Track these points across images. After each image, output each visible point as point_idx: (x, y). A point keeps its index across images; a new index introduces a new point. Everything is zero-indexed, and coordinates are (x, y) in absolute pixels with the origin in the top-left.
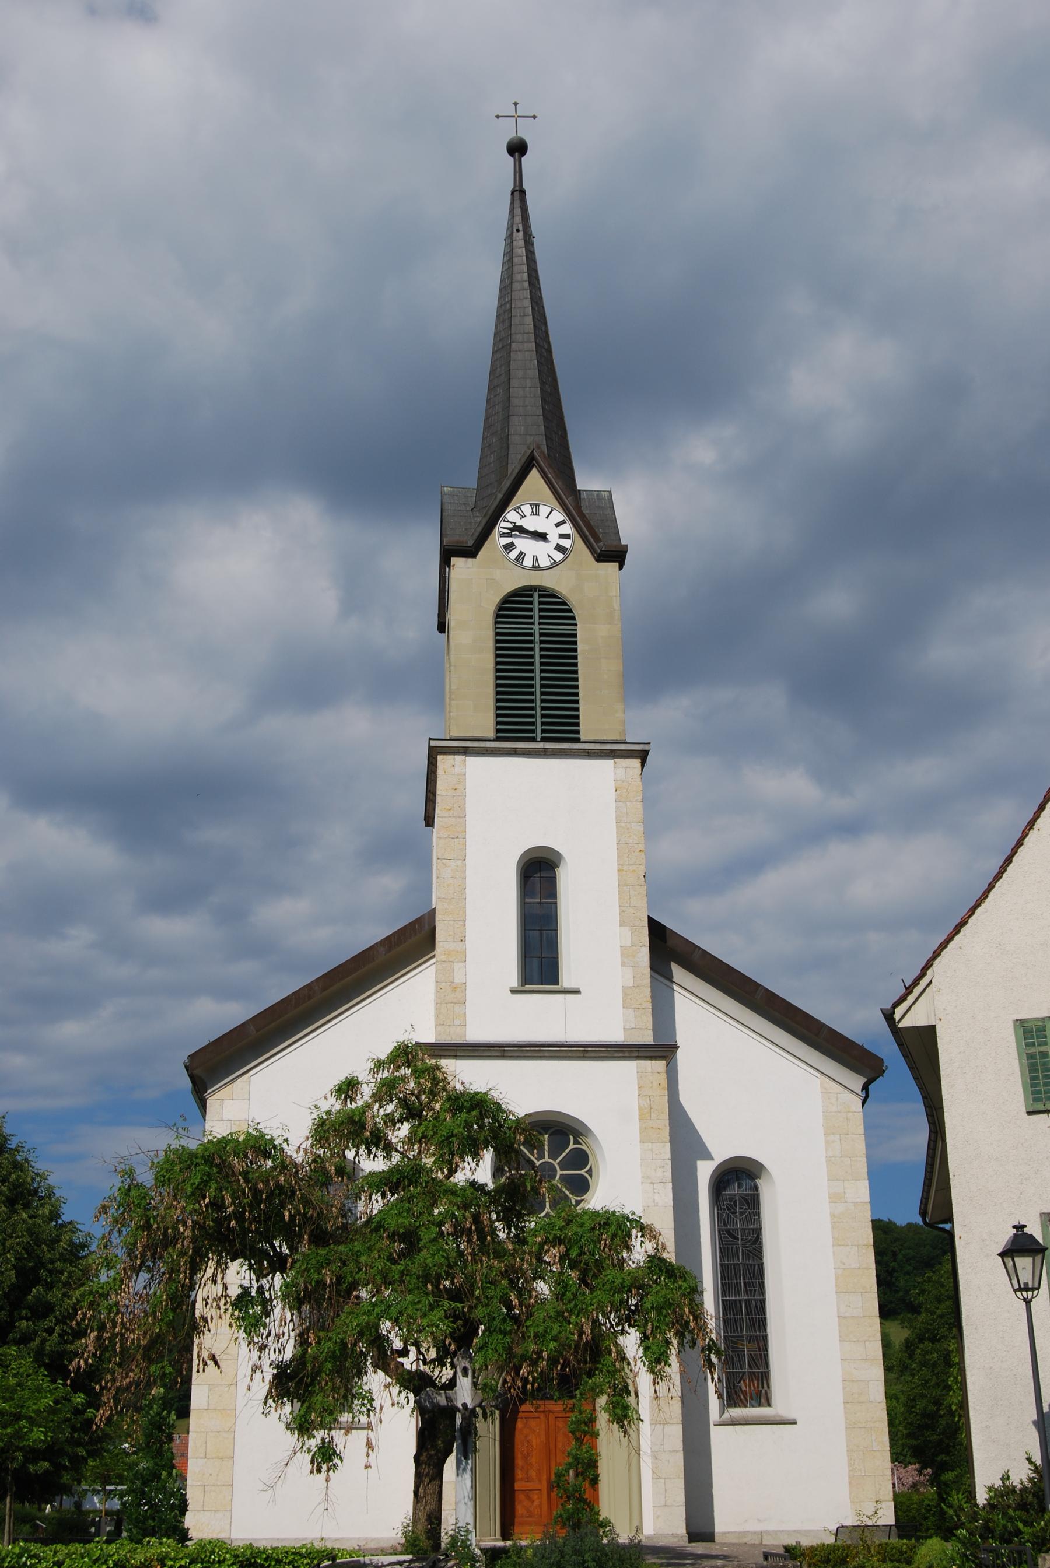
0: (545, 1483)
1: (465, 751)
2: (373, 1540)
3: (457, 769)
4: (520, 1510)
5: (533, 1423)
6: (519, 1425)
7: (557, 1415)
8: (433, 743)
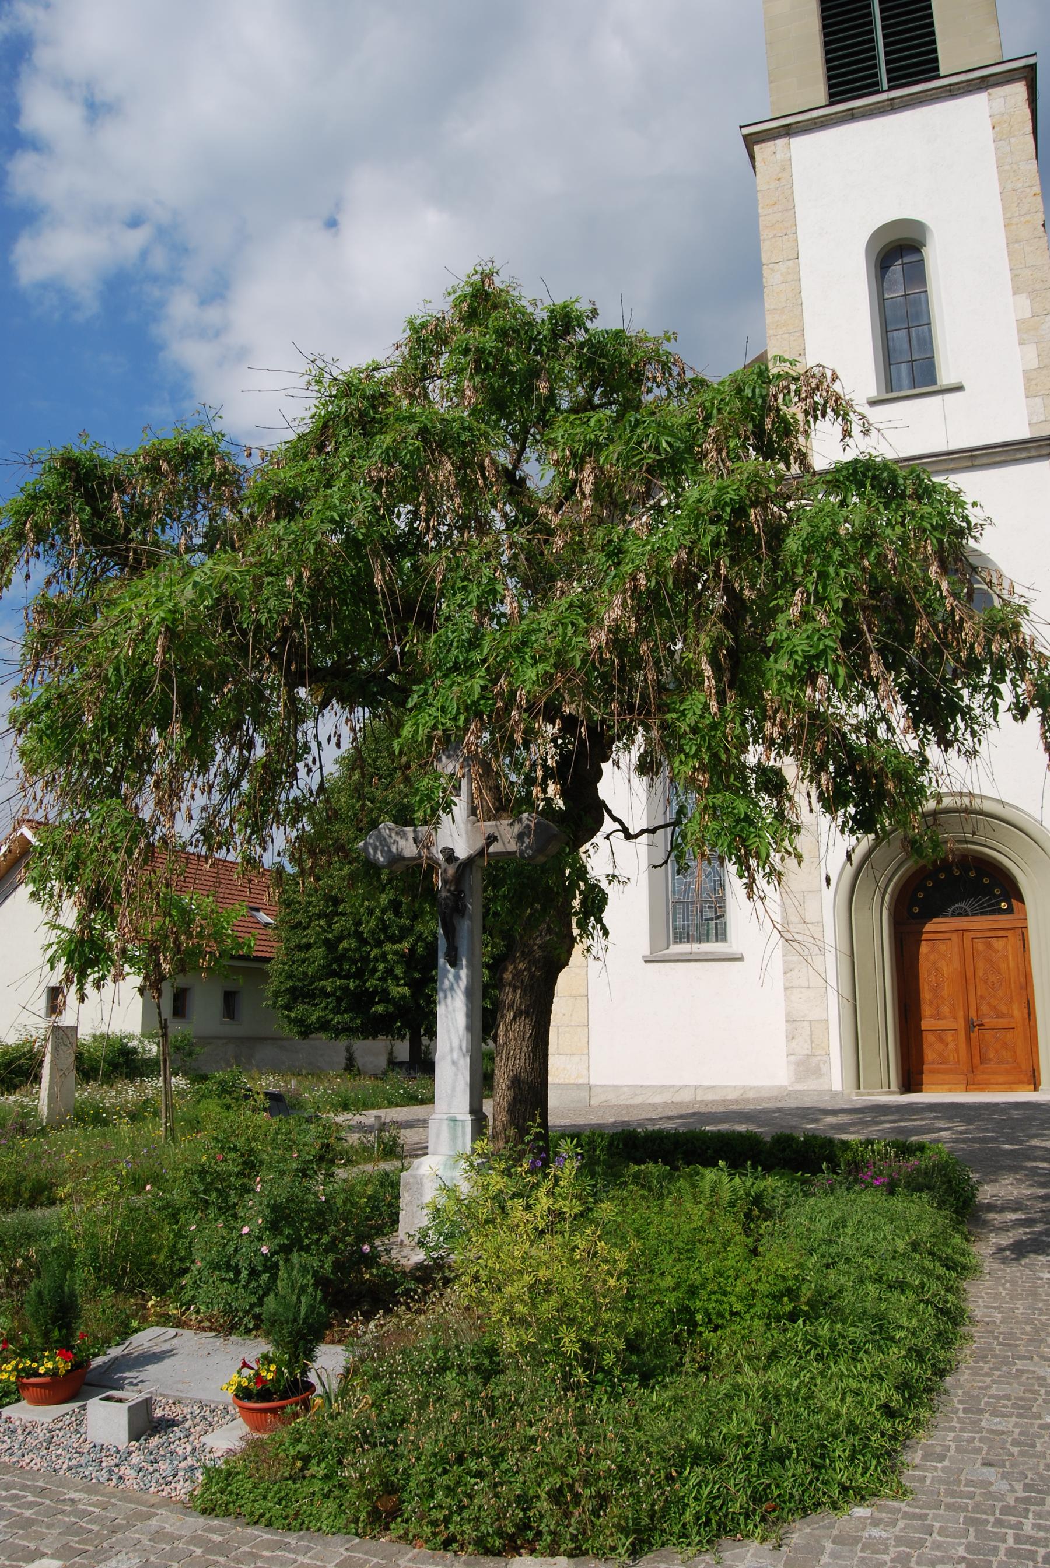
0: (962, 1021)
1: (788, 131)
2: (751, 1088)
3: (779, 156)
4: (929, 1055)
5: (942, 947)
6: (924, 949)
7: (973, 935)
8: (746, 131)
